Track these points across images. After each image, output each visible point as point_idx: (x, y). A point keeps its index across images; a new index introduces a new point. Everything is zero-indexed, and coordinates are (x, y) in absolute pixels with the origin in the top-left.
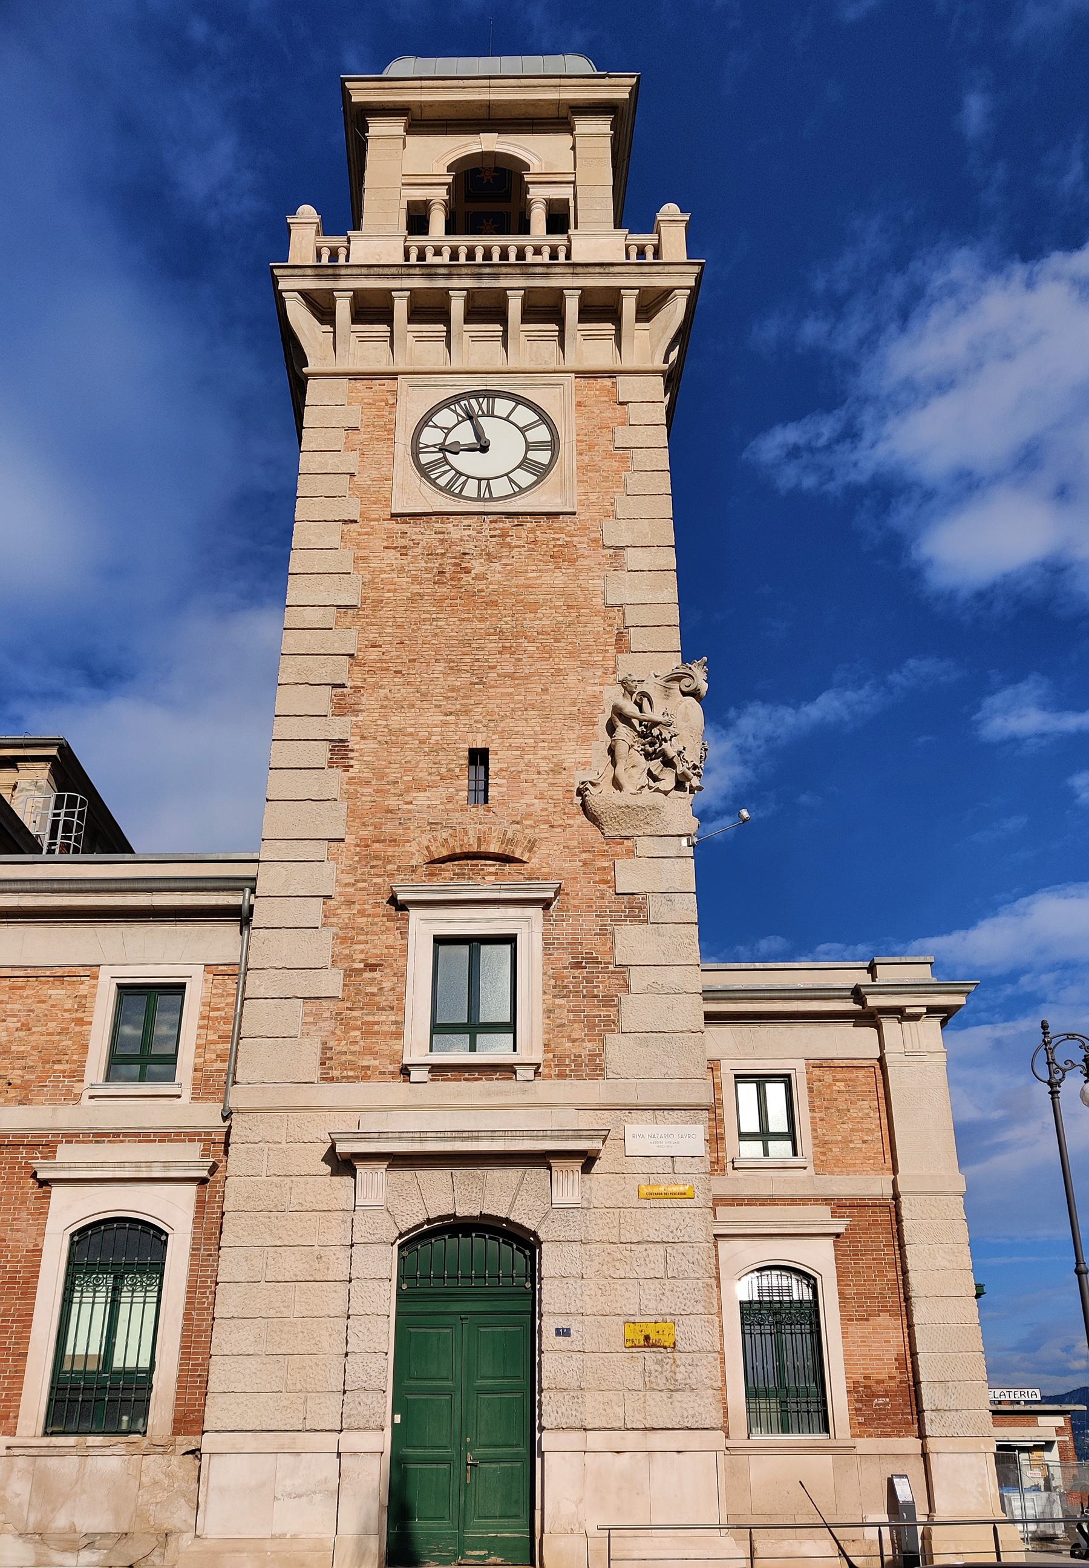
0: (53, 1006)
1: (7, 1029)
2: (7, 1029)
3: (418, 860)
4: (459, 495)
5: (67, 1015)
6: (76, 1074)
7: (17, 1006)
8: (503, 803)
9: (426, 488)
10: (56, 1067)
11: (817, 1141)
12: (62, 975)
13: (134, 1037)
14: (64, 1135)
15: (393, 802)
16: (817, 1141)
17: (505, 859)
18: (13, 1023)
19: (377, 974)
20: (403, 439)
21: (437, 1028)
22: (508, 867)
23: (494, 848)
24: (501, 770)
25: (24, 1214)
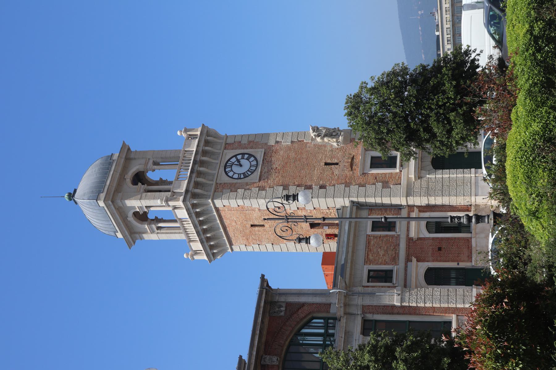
0: (375, 243)
1: (381, 251)
2: (381, 251)
3: (351, 173)
4: (255, 170)
5: (378, 240)
6: (392, 236)
7: (375, 250)
8: (338, 159)
9: (255, 173)
10: (390, 240)
11: (271, 146)
12: (368, 242)
13: (371, 280)
14: (407, 237)
15: (336, 177)
16: (271, 146)
17: (353, 158)
18: (379, 250)
19: (378, 177)
20: (236, 181)
21: (447, 34)
22: (354, 158)
23: (350, 160)
24: (330, 160)
25: (425, 242)
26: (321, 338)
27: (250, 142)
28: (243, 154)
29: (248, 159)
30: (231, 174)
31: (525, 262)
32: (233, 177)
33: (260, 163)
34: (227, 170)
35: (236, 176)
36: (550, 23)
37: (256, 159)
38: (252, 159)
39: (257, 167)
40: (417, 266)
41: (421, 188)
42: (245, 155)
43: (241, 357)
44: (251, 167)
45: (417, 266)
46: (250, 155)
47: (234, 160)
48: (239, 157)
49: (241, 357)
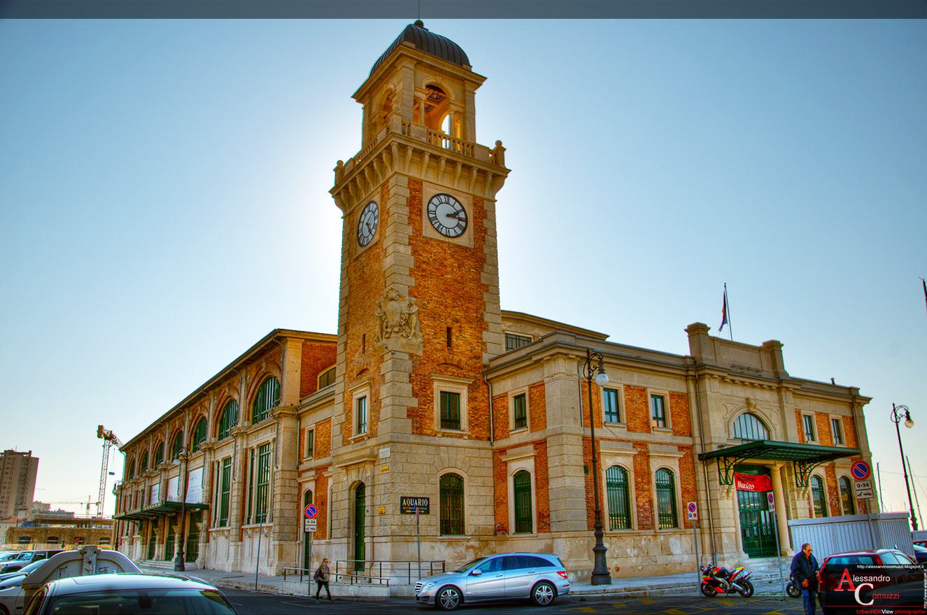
4: (440, 233)
26: (613, 417)
27: (485, 231)
28: (466, 220)
29: (458, 225)
30: (435, 201)
31: (846, 591)
32: (430, 204)
33: (455, 241)
34: (442, 197)
35: (432, 207)
36: (921, 558)
37: (458, 236)
38: (459, 231)
39: (446, 236)
40: (629, 455)
41: (447, 364)
42: (465, 223)
43: (608, 336)
44: (446, 228)
45: (629, 455)
46: (464, 230)
47: (458, 207)
48: (462, 215)
49: (608, 336)
